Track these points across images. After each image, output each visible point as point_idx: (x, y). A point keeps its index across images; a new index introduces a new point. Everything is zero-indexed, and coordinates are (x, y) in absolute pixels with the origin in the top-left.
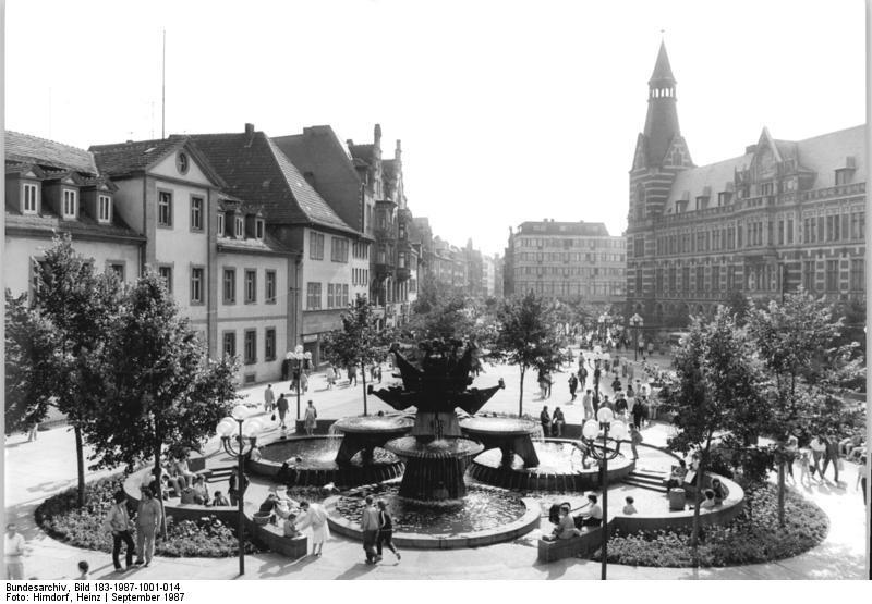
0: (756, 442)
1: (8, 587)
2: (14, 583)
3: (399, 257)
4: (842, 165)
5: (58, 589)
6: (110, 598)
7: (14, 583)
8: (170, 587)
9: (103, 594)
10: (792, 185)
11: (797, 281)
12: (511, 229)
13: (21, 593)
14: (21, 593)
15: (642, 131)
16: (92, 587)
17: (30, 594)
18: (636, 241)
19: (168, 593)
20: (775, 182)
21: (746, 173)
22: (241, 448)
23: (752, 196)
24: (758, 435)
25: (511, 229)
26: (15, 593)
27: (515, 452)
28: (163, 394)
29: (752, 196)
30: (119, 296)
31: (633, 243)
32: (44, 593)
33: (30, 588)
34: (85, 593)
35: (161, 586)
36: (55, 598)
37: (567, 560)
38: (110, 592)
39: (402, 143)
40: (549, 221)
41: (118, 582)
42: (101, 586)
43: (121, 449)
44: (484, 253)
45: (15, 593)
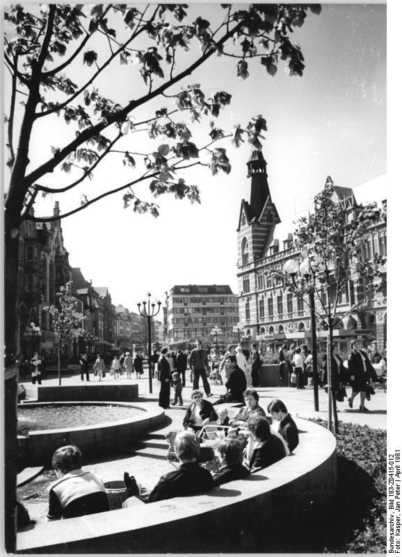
0: (258, 10)
1: (391, 552)
3: (360, 281)
4: (286, 238)
5: (392, 520)
8: (391, 461)
11: (48, 315)
13: (395, 544)
14: (395, 544)
15: (248, 199)
17: (396, 538)
22: (347, 207)
24: (362, 391)
26: (395, 547)
27: (345, 384)
32: (395, 529)
33: (392, 538)
36: (398, 525)
40: (55, 104)
43: (214, 472)
45: (395, 547)
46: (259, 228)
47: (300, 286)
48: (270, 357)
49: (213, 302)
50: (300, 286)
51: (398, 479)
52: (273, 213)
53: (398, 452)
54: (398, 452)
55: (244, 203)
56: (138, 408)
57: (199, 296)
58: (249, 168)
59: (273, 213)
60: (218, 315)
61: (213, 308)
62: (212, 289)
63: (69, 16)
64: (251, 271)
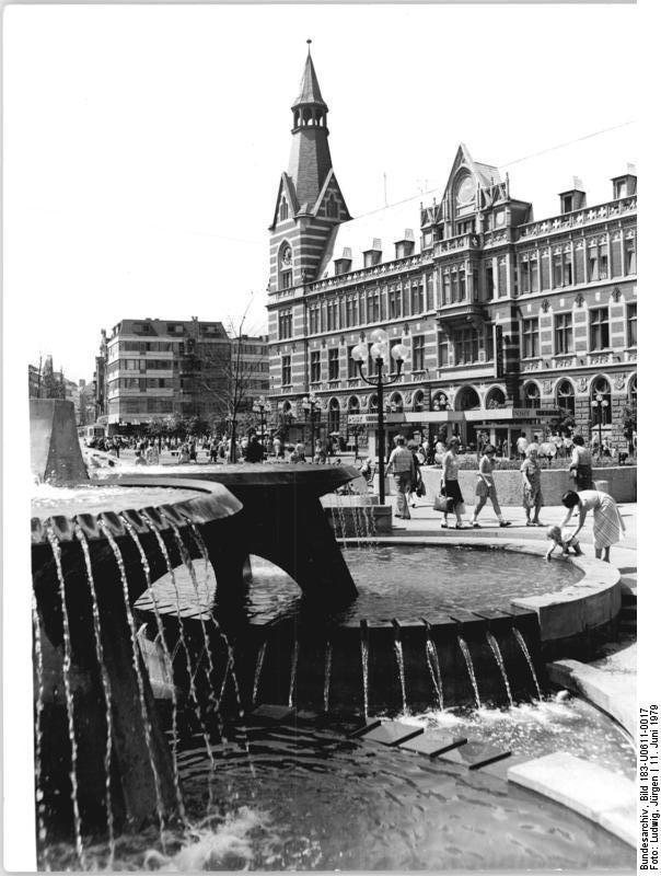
1: (644, 867)
2: (640, 862)
6: (655, 766)
7: (640, 862)
8: (645, 718)
9: (651, 774)
10: (502, 219)
12: (104, 332)
13: (650, 855)
14: (650, 855)
16: (644, 783)
18: (280, 318)
19: (650, 721)
20: (479, 219)
21: (438, 210)
23: (445, 239)
25: (104, 332)
26: (650, 860)
28: (211, 701)
29: (445, 239)
30: (439, 446)
31: (277, 322)
34: (650, 791)
35: (642, 732)
37: (39, 772)
38: (650, 767)
39: (336, 123)
41: (639, 758)
42: (643, 774)
44: (68, 377)
45: (650, 860)
52: (339, 201)
64: (298, 301)
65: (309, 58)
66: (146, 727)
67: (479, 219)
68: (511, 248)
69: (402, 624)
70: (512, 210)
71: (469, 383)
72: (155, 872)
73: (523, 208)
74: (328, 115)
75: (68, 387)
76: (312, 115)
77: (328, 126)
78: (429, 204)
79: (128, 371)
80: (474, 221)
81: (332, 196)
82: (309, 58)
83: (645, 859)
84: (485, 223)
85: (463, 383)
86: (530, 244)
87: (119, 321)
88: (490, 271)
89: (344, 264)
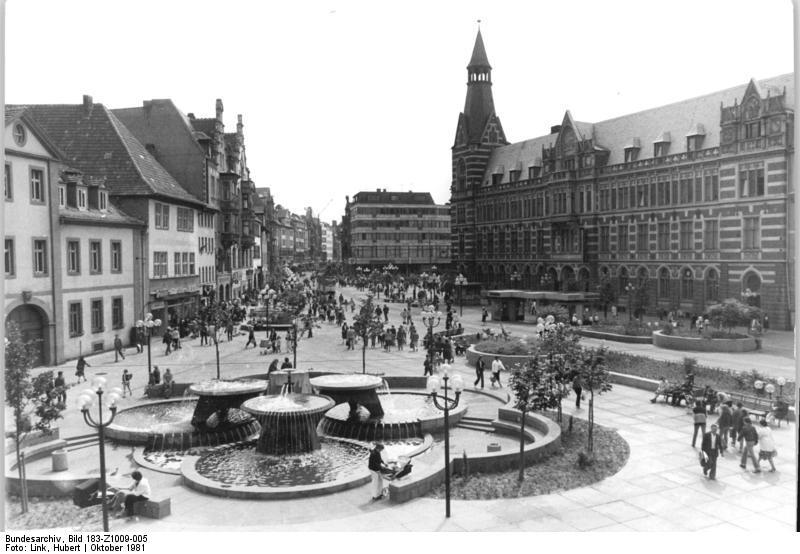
1: (8, 538)
10: (590, 161)
12: (347, 198)
13: (19, 544)
14: (19, 544)
20: (576, 159)
21: (552, 151)
25: (347, 198)
26: (14, 544)
37: (214, 394)
44: (323, 220)
45: (14, 544)
46: (481, 150)
47: (456, 254)
48: (687, 323)
49: (155, 266)
50: (456, 254)
51: (88, 548)
52: (497, 132)
53: (141, 548)
54: (141, 548)
55: (461, 114)
56: (54, 312)
57: (390, 206)
58: (470, 73)
59: (497, 132)
60: (415, 230)
61: (407, 222)
62: (410, 197)
63: (109, 151)
64: (468, 199)
65: (479, 35)
66: (371, 444)
67: (576, 159)
68: (595, 180)
69: (469, 456)
70: (596, 156)
71: (570, 264)
72: (194, 105)
73: (603, 154)
74: (492, 72)
75: (323, 228)
76: (479, 65)
77: (492, 81)
78: (547, 147)
79: (366, 241)
80: (574, 160)
81: (493, 129)
82: (479, 35)
83: (16, 539)
84: (580, 162)
85: (565, 264)
86: (606, 179)
87: (357, 192)
88: (582, 194)
89: (497, 178)
